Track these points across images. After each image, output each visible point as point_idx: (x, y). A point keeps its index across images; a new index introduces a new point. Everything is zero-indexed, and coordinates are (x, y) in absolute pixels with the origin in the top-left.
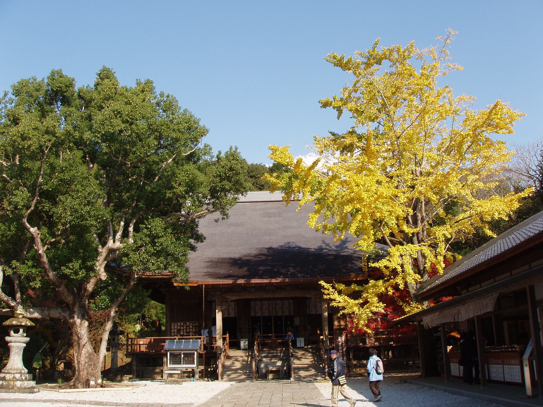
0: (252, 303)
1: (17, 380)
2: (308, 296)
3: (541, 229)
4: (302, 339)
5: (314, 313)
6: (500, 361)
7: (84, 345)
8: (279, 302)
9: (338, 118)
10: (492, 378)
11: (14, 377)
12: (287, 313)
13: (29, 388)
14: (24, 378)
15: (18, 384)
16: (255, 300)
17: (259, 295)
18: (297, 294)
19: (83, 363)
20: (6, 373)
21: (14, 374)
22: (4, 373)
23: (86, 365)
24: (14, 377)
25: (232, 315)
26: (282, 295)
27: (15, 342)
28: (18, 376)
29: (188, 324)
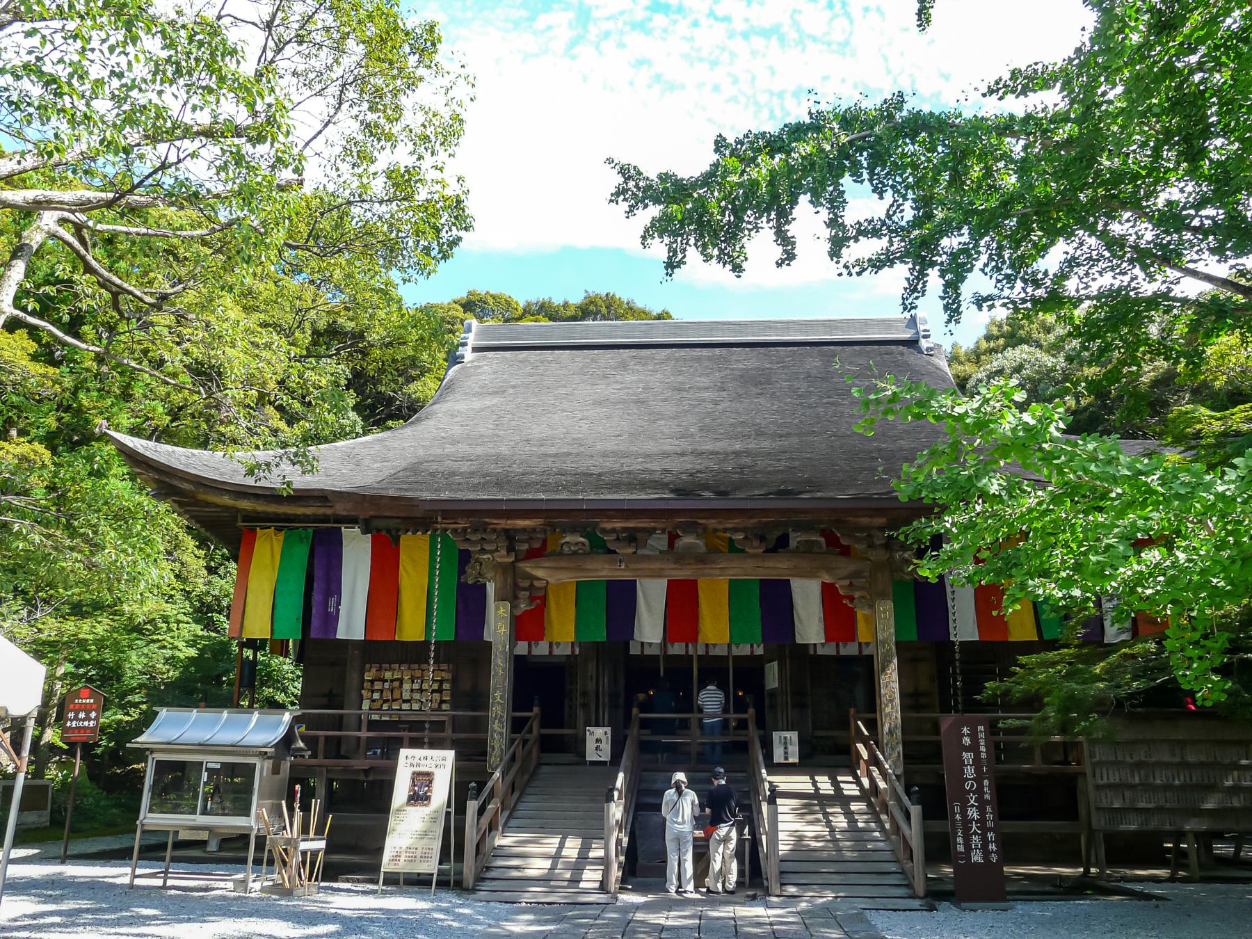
4: (793, 736)
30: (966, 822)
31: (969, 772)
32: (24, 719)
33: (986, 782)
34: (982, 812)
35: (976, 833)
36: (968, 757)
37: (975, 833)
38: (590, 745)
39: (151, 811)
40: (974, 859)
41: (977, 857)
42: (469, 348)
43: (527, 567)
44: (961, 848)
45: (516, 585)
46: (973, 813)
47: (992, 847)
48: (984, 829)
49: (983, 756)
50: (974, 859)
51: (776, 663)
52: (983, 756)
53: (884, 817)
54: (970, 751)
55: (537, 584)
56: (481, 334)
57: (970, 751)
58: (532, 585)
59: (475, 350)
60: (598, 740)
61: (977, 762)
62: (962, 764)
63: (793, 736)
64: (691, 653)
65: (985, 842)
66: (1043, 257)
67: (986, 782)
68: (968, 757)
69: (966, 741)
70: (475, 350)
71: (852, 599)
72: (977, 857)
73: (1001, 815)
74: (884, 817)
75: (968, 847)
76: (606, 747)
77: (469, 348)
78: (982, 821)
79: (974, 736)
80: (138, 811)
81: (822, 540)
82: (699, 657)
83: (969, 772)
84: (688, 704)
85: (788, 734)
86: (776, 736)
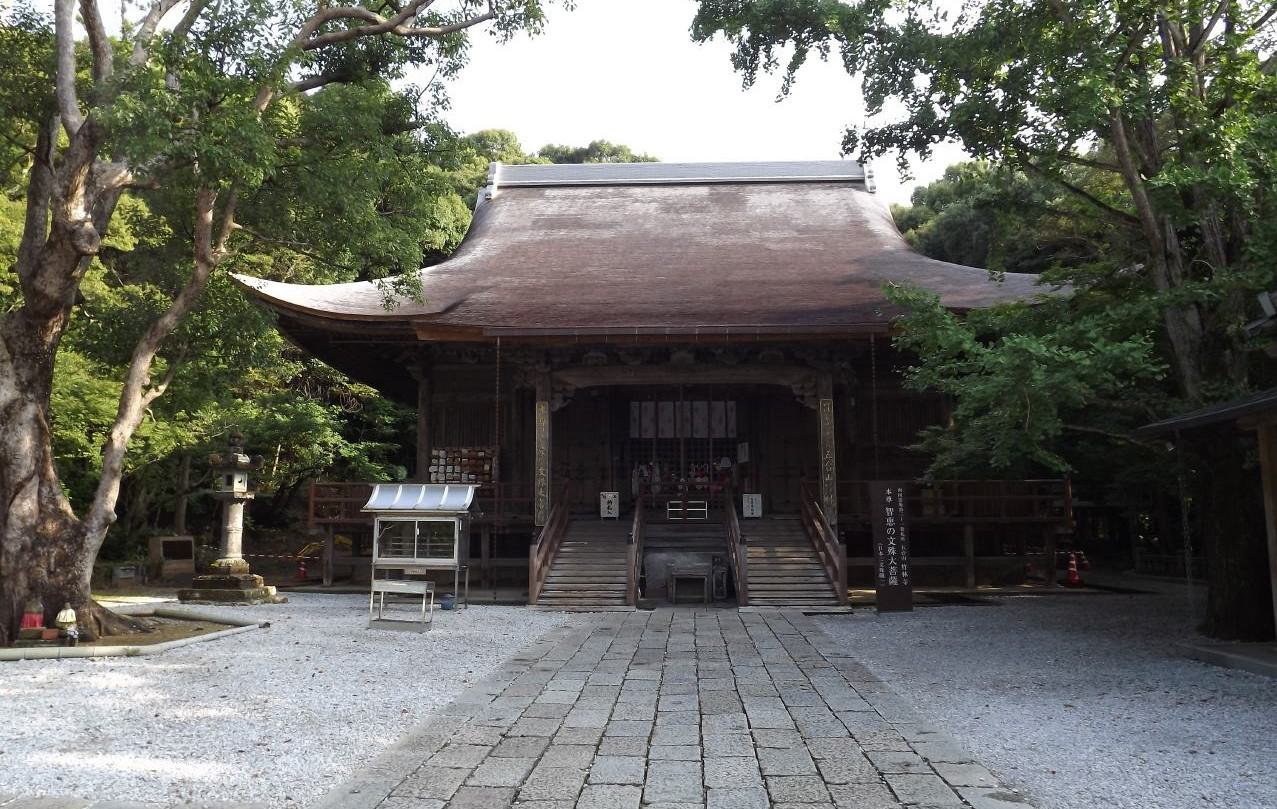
4: (758, 498)
18: (753, 376)
30: (887, 557)
31: (890, 521)
32: (562, 531)
33: (902, 529)
34: (898, 549)
35: (893, 560)
36: (890, 511)
37: (893, 565)
38: (604, 506)
39: (379, 556)
40: (891, 583)
41: (893, 581)
42: (495, 187)
43: (561, 375)
44: (882, 576)
45: (553, 389)
46: (892, 551)
47: (905, 574)
48: (899, 562)
49: (901, 510)
50: (891, 583)
51: (747, 444)
52: (901, 510)
53: (822, 554)
54: (891, 504)
55: (568, 388)
56: (505, 174)
57: (891, 504)
58: (564, 389)
59: (500, 187)
60: (610, 502)
61: (896, 515)
62: (886, 516)
63: (758, 498)
64: (678, 436)
65: (900, 571)
66: (629, 150)
67: (902, 529)
68: (890, 511)
69: (889, 499)
70: (500, 187)
71: (802, 397)
72: (893, 581)
73: (913, 552)
74: (822, 554)
75: (887, 576)
76: (615, 506)
77: (495, 187)
78: (898, 556)
79: (894, 496)
80: (371, 556)
81: (604, 356)
82: (716, 441)
83: (890, 521)
84: (246, 452)
85: (755, 496)
86: (746, 497)
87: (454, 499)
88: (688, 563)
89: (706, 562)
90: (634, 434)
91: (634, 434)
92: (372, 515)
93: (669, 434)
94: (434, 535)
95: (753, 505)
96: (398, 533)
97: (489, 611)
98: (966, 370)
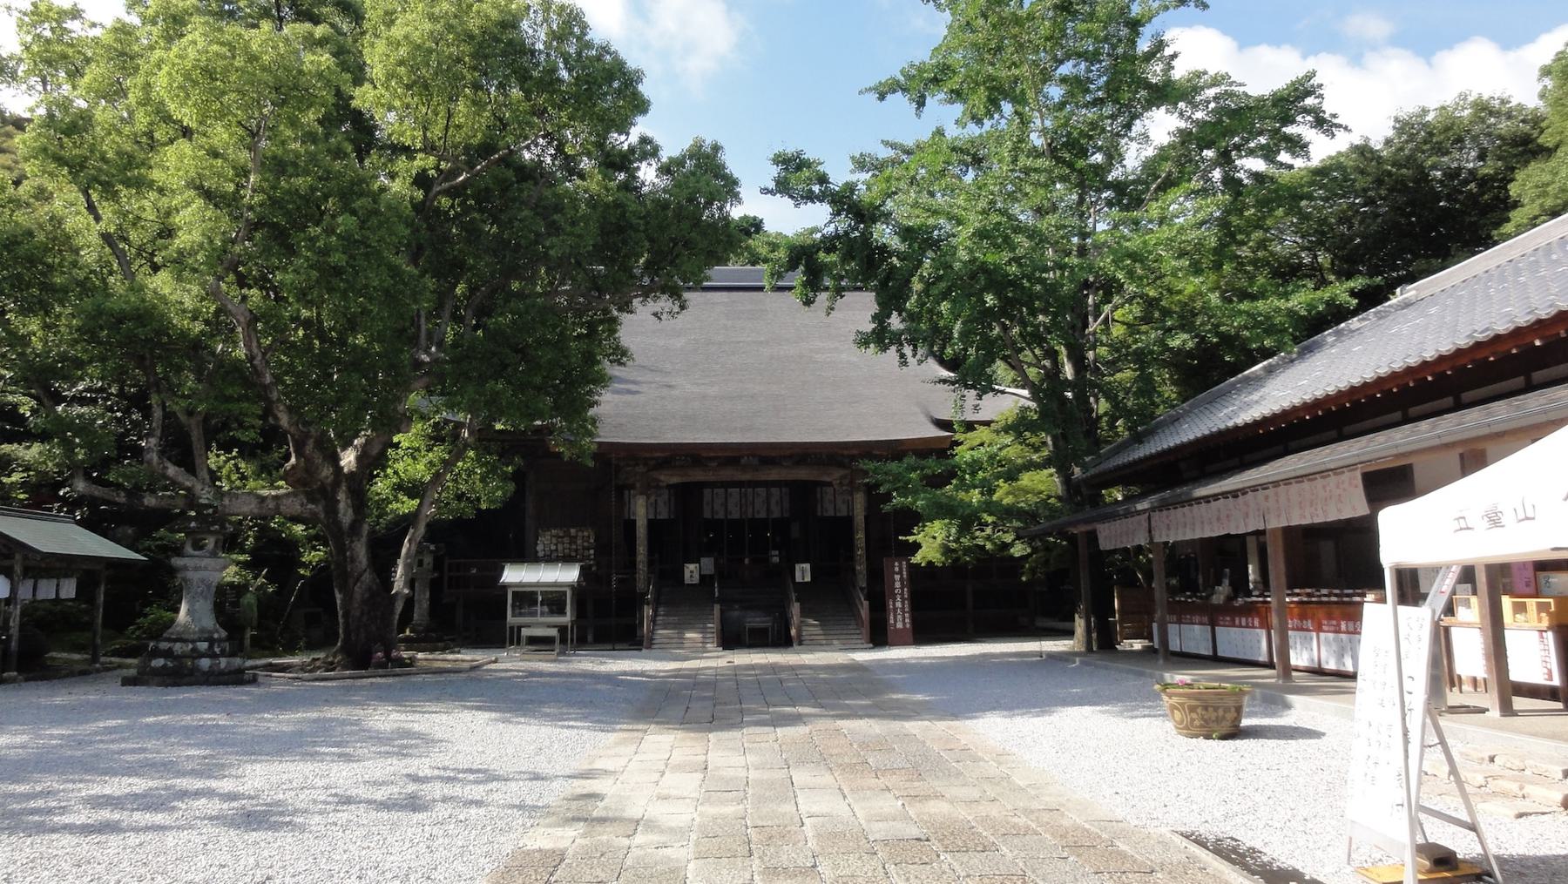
0: (707, 492)
1: (203, 655)
2: (827, 479)
3: (1564, 305)
4: (807, 566)
5: (831, 513)
6: (1205, 619)
7: (480, 680)
8: (762, 491)
9: (918, 116)
10: (1220, 653)
11: (194, 650)
12: (776, 514)
13: (230, 673)
14: (217, 650)
15: (205, 663)
16: (712, 485)
17: (728, 474)
18: (802, 474)
19: (358, 614)
20: (176, 641)
21: (193, 641)
22: (169, 640)
23: (365, 619)
24: (194, 650)
25: (664, 515)
26: (774, 474)
27: (196, 569)
28: (203, 646)
29: (573, 531)
31: (898, 585)
36: (897, 577)
38: (687, 575)
43: (655, 474)
46: (899, 605)
61: (902, 579)
68: (897, 577)
83: (898, 585)
86: (798, 567)
87: (568, 575)
88: (756, 620)
89: (54, 659)
90: (707, 515)
91: (707, 515)
92: (505, 587)
93: (736, 515)
94: (553, 599)
95: (803, 573)
96: (526, 597)
97: (1468, 418)
98: (519, 819)
